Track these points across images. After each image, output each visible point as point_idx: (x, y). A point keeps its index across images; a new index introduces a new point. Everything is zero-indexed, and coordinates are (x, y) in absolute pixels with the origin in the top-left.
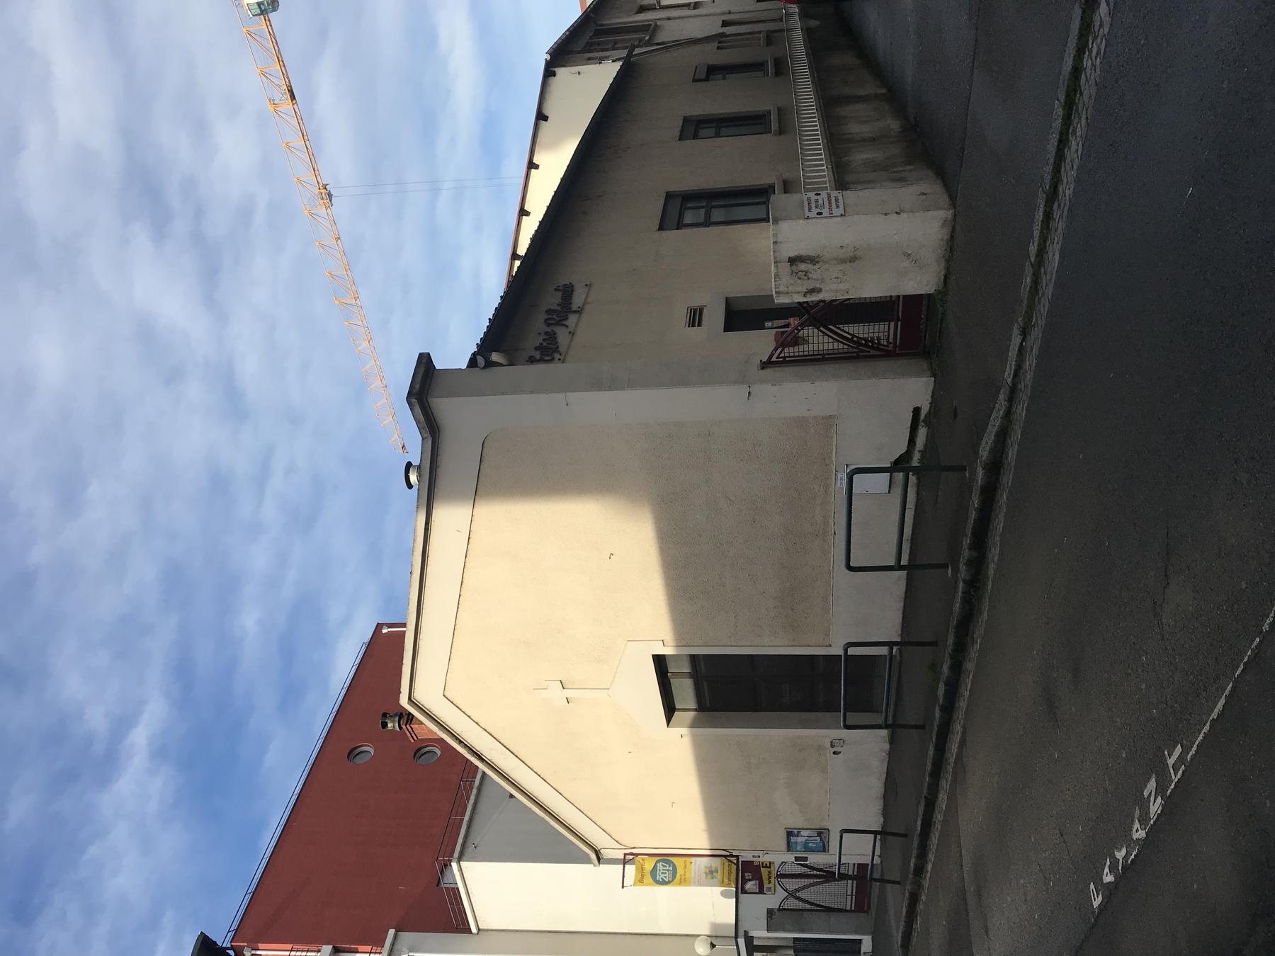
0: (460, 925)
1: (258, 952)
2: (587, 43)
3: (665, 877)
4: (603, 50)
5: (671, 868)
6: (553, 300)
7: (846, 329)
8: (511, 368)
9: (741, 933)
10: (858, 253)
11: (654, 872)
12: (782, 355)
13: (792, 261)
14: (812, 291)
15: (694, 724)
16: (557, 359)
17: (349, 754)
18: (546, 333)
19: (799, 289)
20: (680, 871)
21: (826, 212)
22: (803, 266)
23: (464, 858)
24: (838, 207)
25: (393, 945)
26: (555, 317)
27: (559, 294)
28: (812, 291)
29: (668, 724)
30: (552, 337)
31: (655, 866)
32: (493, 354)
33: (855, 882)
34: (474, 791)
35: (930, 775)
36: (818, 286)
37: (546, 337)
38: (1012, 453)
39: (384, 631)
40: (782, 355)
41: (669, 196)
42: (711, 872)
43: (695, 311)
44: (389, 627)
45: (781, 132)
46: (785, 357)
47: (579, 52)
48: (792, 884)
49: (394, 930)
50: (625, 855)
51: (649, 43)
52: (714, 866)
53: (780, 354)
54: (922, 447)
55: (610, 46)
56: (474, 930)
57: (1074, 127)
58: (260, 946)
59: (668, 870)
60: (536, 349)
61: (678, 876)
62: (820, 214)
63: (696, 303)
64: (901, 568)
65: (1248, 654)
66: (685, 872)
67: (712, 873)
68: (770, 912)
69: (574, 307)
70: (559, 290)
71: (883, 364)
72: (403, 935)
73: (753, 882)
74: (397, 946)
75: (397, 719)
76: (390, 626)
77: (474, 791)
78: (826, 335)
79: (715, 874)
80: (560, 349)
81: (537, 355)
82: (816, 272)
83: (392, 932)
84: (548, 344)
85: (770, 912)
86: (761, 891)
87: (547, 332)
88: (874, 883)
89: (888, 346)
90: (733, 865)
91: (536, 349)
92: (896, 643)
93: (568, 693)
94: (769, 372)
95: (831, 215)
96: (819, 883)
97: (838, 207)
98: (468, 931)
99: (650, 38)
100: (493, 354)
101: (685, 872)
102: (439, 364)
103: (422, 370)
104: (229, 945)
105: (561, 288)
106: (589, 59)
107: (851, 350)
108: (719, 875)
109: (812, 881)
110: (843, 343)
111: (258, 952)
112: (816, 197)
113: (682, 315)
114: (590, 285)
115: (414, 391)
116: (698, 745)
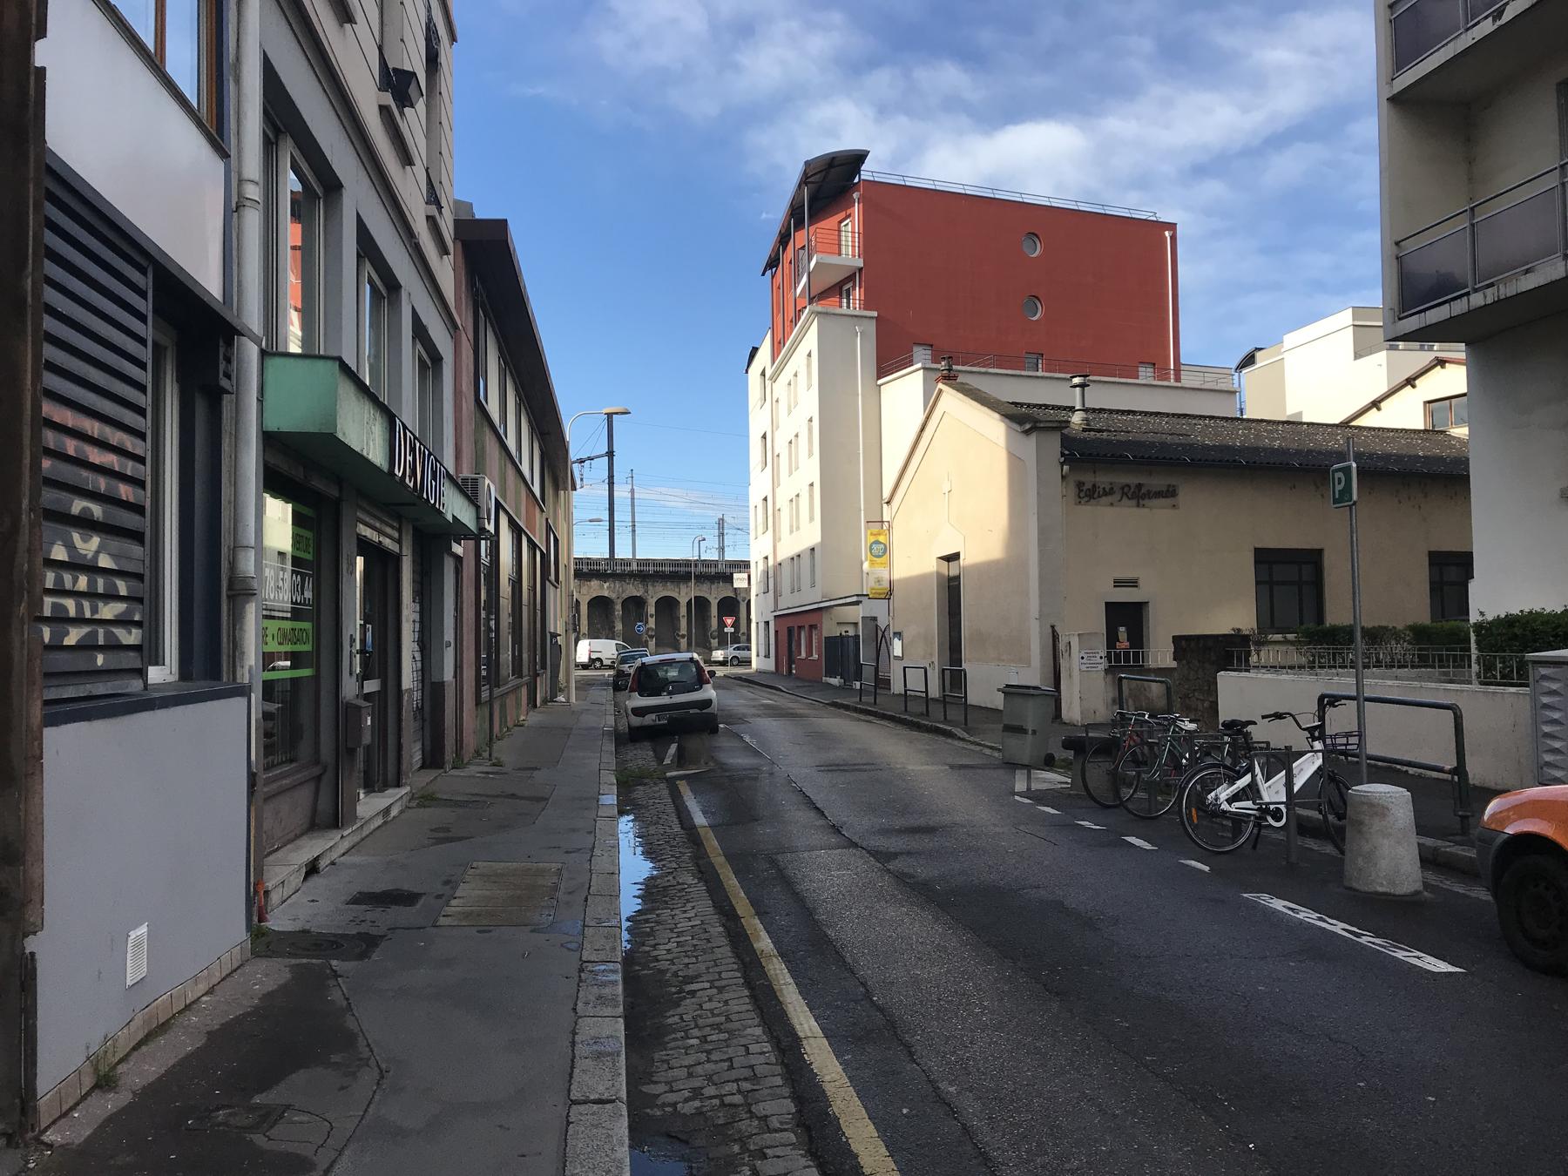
0: (883, 371)
1: (856, 204)
8: (1060, 477)
9: (860, 599)
11: (877, 542)
15: (939, 575)
17: (1033, 234)
20: (878, 560)
23: (926, 372)
25: (866, 317)
29: (940, 558)
31: (881, 543)
32: (1068, 467)
34: (983, 370)
38: (956, 743)
39: (1167, 233)
42: (879, 581)
43: (1136, 582)
44: (1171, 238)
52: (884, 583)
54: (1477, 783)
56: (880, 382)
58: (861, 205)
61: (875, 559)
63: (1141, 583)
64: (906, 691)
65: (699, 711)
68: (875, 619)
74: (865, 321)
75: (947, 368)
76: (1173, 238)
77: (983, 370)
80: (1092, 500)
81: (1088, 486)
83: (875, 314)
85: (875, 619)
91: (1094, 486)
92: (966, 700)
98: (879, 378)
100: (1068, 467)
104: (862, 177)
108: (877, 587)
111: (856, 204)
116: (930, 575)
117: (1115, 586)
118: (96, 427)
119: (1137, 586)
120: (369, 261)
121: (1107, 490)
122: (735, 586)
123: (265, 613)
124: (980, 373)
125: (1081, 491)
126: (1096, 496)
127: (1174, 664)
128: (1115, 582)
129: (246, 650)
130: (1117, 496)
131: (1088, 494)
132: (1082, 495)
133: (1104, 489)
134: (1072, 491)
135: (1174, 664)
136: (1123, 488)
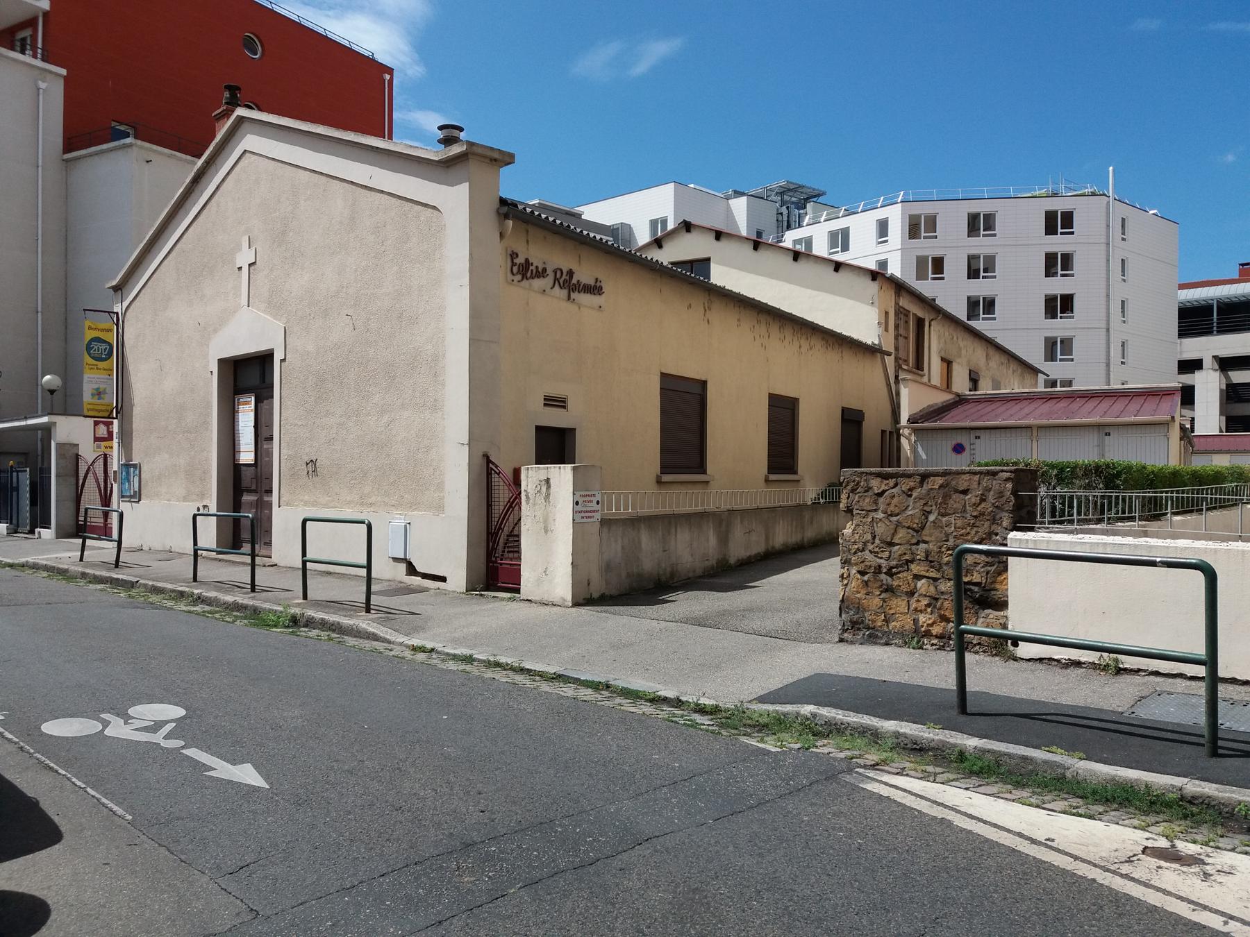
2: (909, 312)
3: (95, 351)
4: (897, 327)
5: (103, 356)
6: (584, 275)
7: (497, 520)
10: (549, 533)
12: (493, 472)
13: (548, 481)
14: (527, 497)
16: (513, 277)
18: (545, 270)
19: (529, 487)
21: (579, 508)
22: (544, 489)
24: (582, 517)
26: (564, 277)
27: (592, 283)
28: (527, 497)
30: (541, 274)
33: (102, 525)
35: (153, 586)
36: (531, 501)
37: (540, 270)
40: (493, 472)
41: (704, 384)
43: (564, 402)
45: (767, 481)
46: (491, 474)
47: (897, 304)
48: (99, 466)
49: (65, 74)
50: (117, 313)
51: (898, 367)
53: (494, 470)
55: (901, 331)
57: (936, 774)
59: (102, 353)
60: (527, 260)
62: (577, 503)
63: (570, 404)
64: (304, 563)
66: (100, 369)
67: (98, 394)
69: (573, 295)
70: (596, 282)
71: (482, 553)
72: (62, 82)
73: (105, 432)
78: (505, 508)
79: (97, 397)
80: (525, 280)
81: (520, 260)
82: (540, 500)
83: (64, 72)
84: (532, 270)
86: (97, 439)
87: (546, 270)
88: (81, 540)
89: (494, 556)
90: (108, 413)
91: (527, 260)
93: (245, 269)
94: (479, 461)
95: (575, 512)
96: (100, 491)
97: (582, 517)
99: (905, 370)
101: (100, 369)
102: (505, 171)
103: (496, 156)
105: (598, 284)
106: (887, 313)
107: (493, 528)
109: (102, 486)
110: (498, 522)
112: (595, 502)
113: (556, 391)
114: (602, 311)
115: (475, 148)
117: (545, 405)
118: (89, 376)
119: (564, 407)
120: (256, 789)
121: (540, 270)
122: (934, 634)
123: (791, 343)
124: (110, 150)
125: (513, 264)
126: (529, 274)
127: (1019, 642)
128: (545, 399)
129: (143, 263)
130: (548, 281)
131: (524, 271)
132: (515, 269)
133: (537, 267)
134: (499, 261)
135: (1019, 642)
136: (555, 272)
